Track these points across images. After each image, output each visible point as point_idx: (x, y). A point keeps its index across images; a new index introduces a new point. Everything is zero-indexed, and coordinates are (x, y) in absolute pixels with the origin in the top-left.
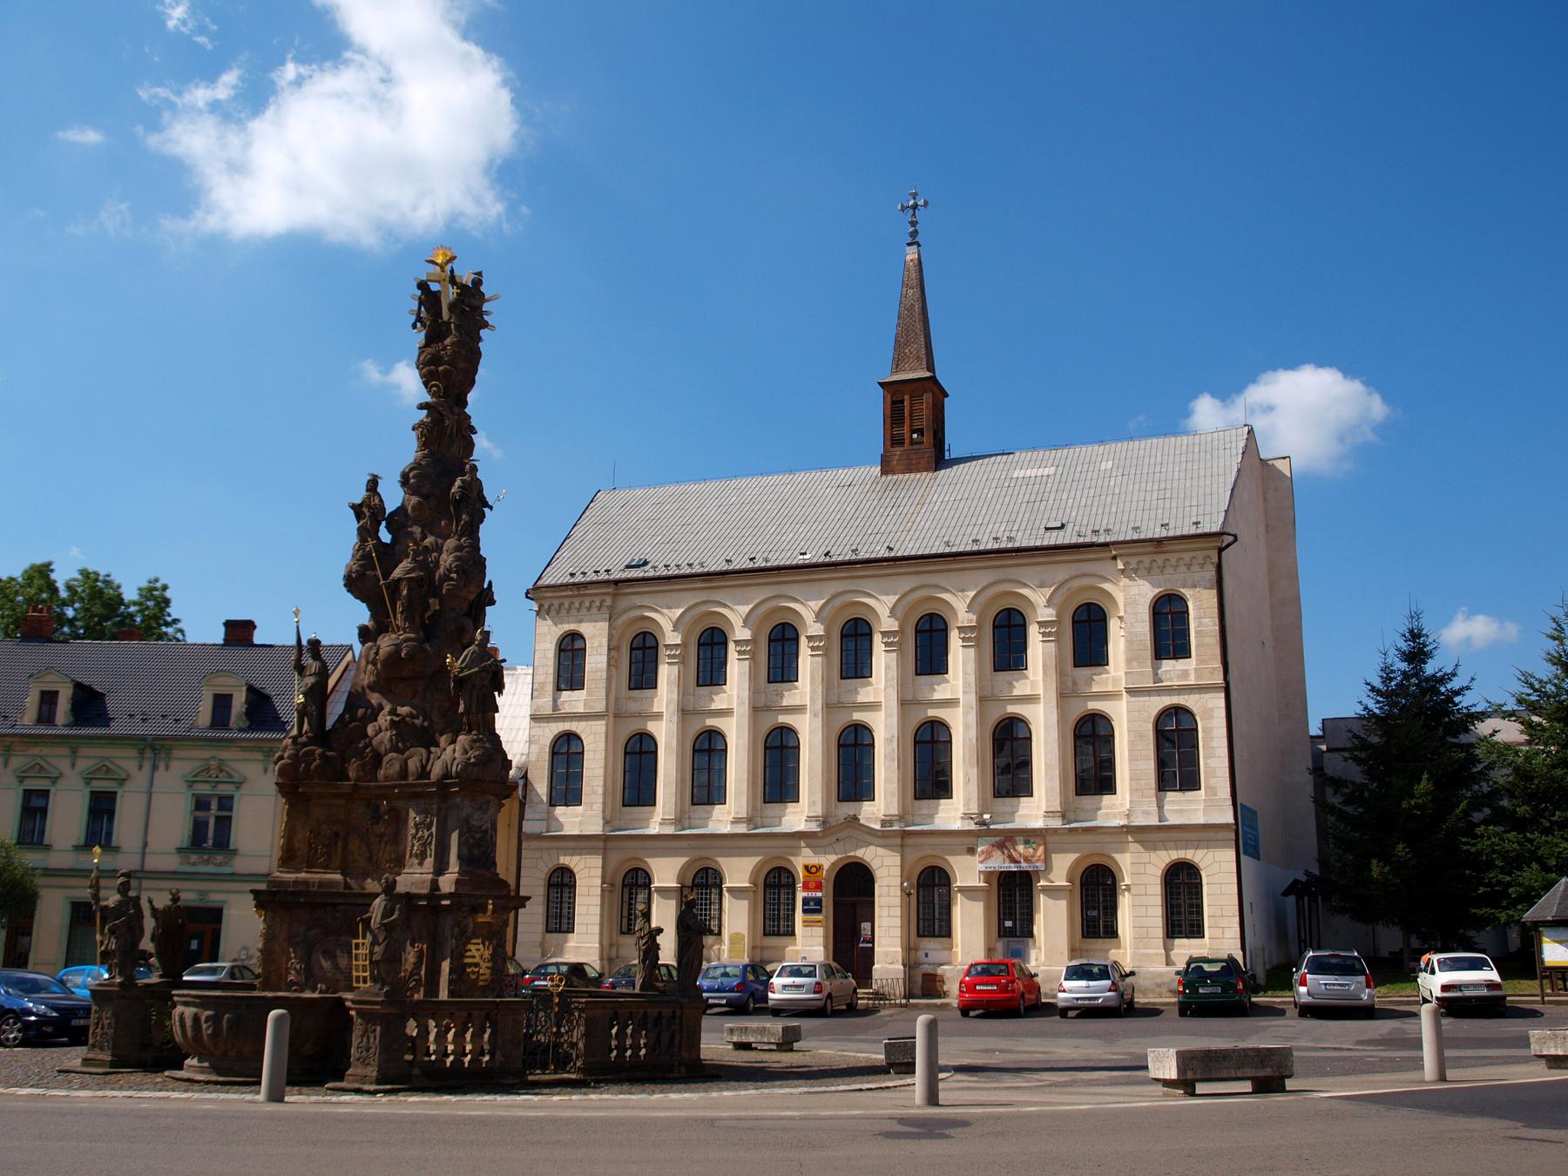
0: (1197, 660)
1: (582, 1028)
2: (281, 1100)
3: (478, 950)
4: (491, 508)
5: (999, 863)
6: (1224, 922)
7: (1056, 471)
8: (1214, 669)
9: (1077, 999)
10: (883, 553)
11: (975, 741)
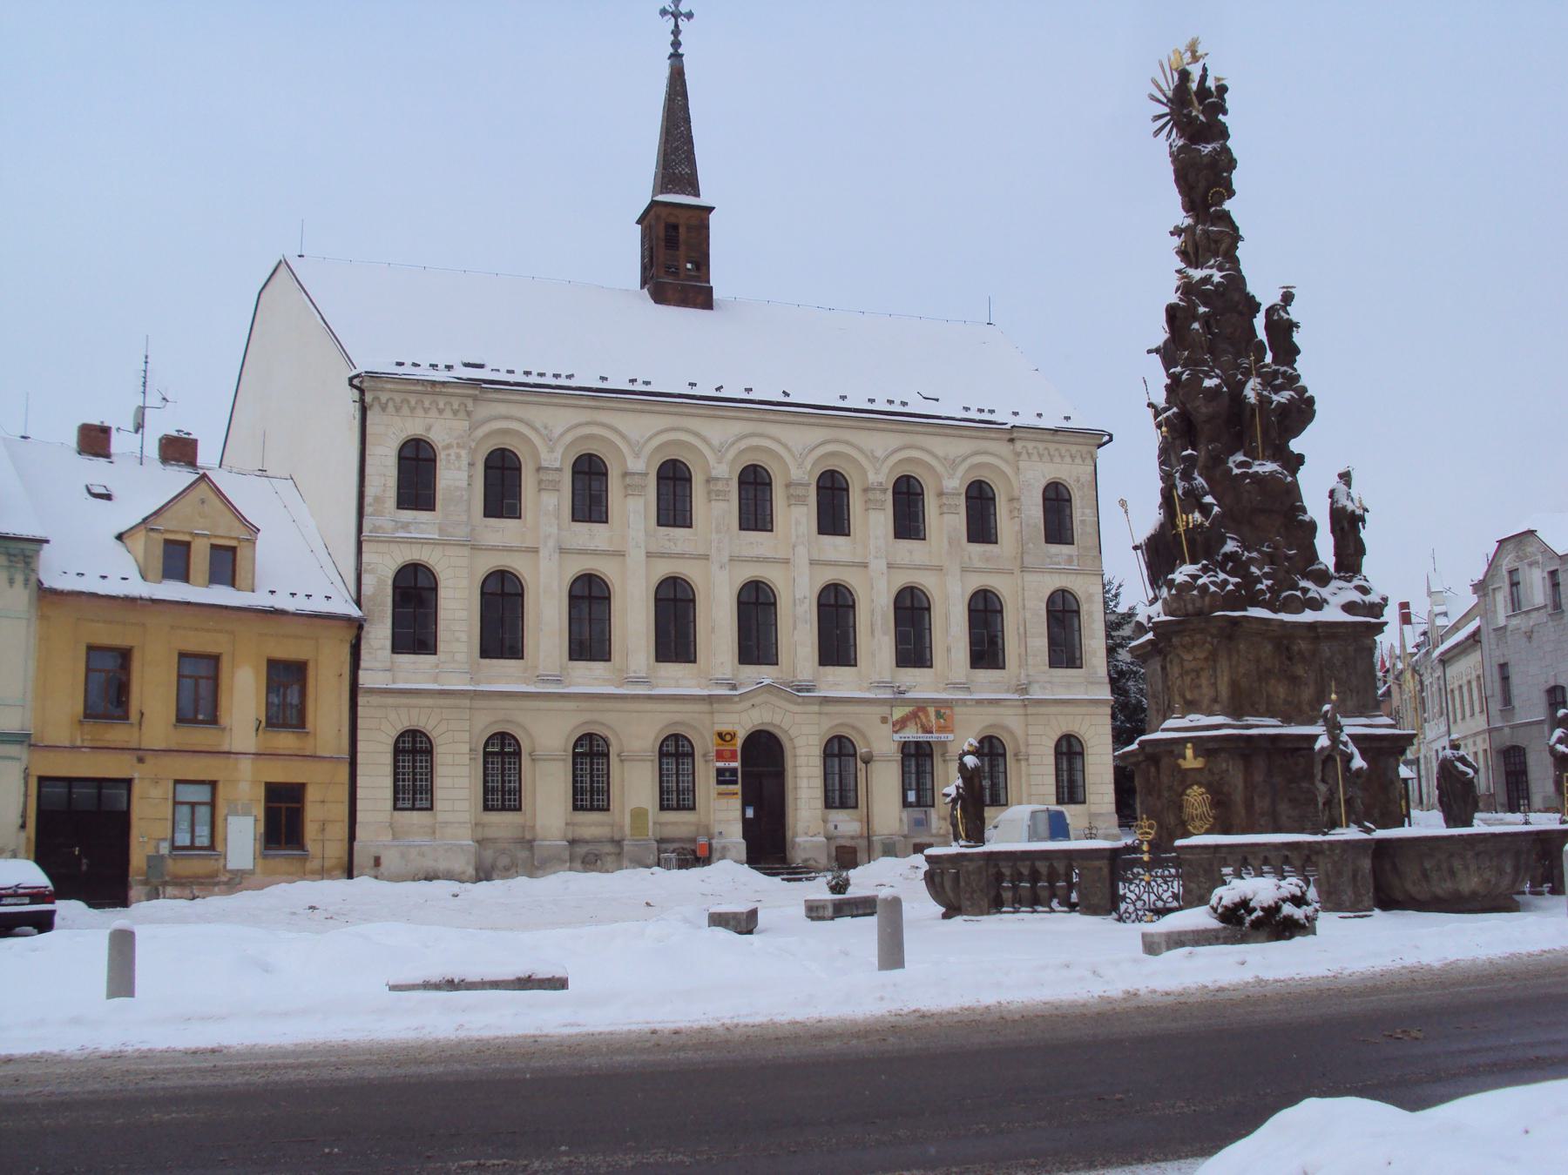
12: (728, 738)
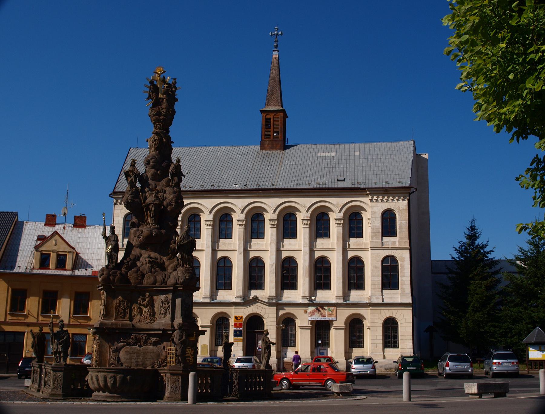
0: (399, 237)
1: (238, 381)
2: (196, 404)
3: (190, 351)
4: (185, 176)
5: (317, 317)
6: (407, 342)
7: (336, 154)
8: (406, 241)
9: (359, 371)
10: (270, 186)
11: (308, 267)
12: (239, 318)
